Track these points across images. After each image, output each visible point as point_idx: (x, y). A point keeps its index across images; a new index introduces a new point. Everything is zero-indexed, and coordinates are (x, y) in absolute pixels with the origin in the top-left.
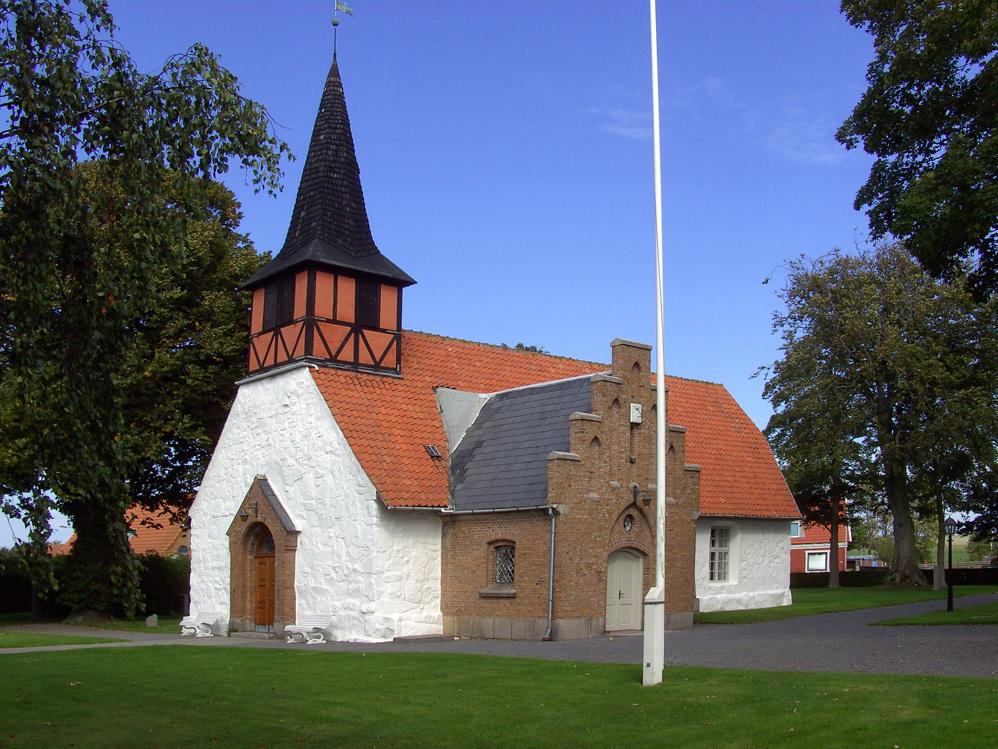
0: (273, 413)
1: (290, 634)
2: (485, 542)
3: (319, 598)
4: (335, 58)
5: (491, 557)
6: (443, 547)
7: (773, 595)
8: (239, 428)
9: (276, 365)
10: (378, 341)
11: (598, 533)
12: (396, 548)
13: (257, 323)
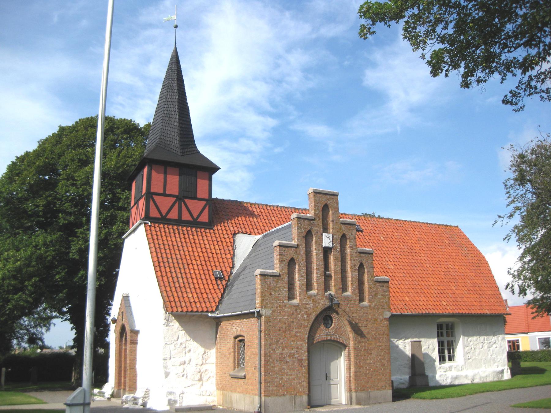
2: (232, 337)
4: (175, 45)
10: (196, 206)
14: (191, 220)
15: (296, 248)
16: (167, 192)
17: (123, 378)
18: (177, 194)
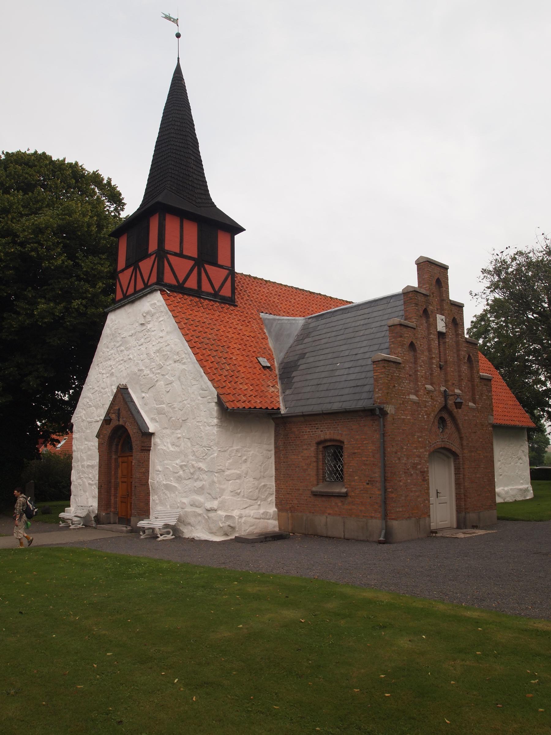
0: (133, 332)
1: (143, 530)
3: (169, 495)
5: (320, 456)
6: (276, 447)
7: (521, 490)
8: (108, 348)
9: (136, 292)
11: (419, 434)
12: (235, 448)
13: (122, 263)
14: (213, 292)
15: (131, 336)
16: (185, 253)
17: (112, 498)
18: (195, 255)
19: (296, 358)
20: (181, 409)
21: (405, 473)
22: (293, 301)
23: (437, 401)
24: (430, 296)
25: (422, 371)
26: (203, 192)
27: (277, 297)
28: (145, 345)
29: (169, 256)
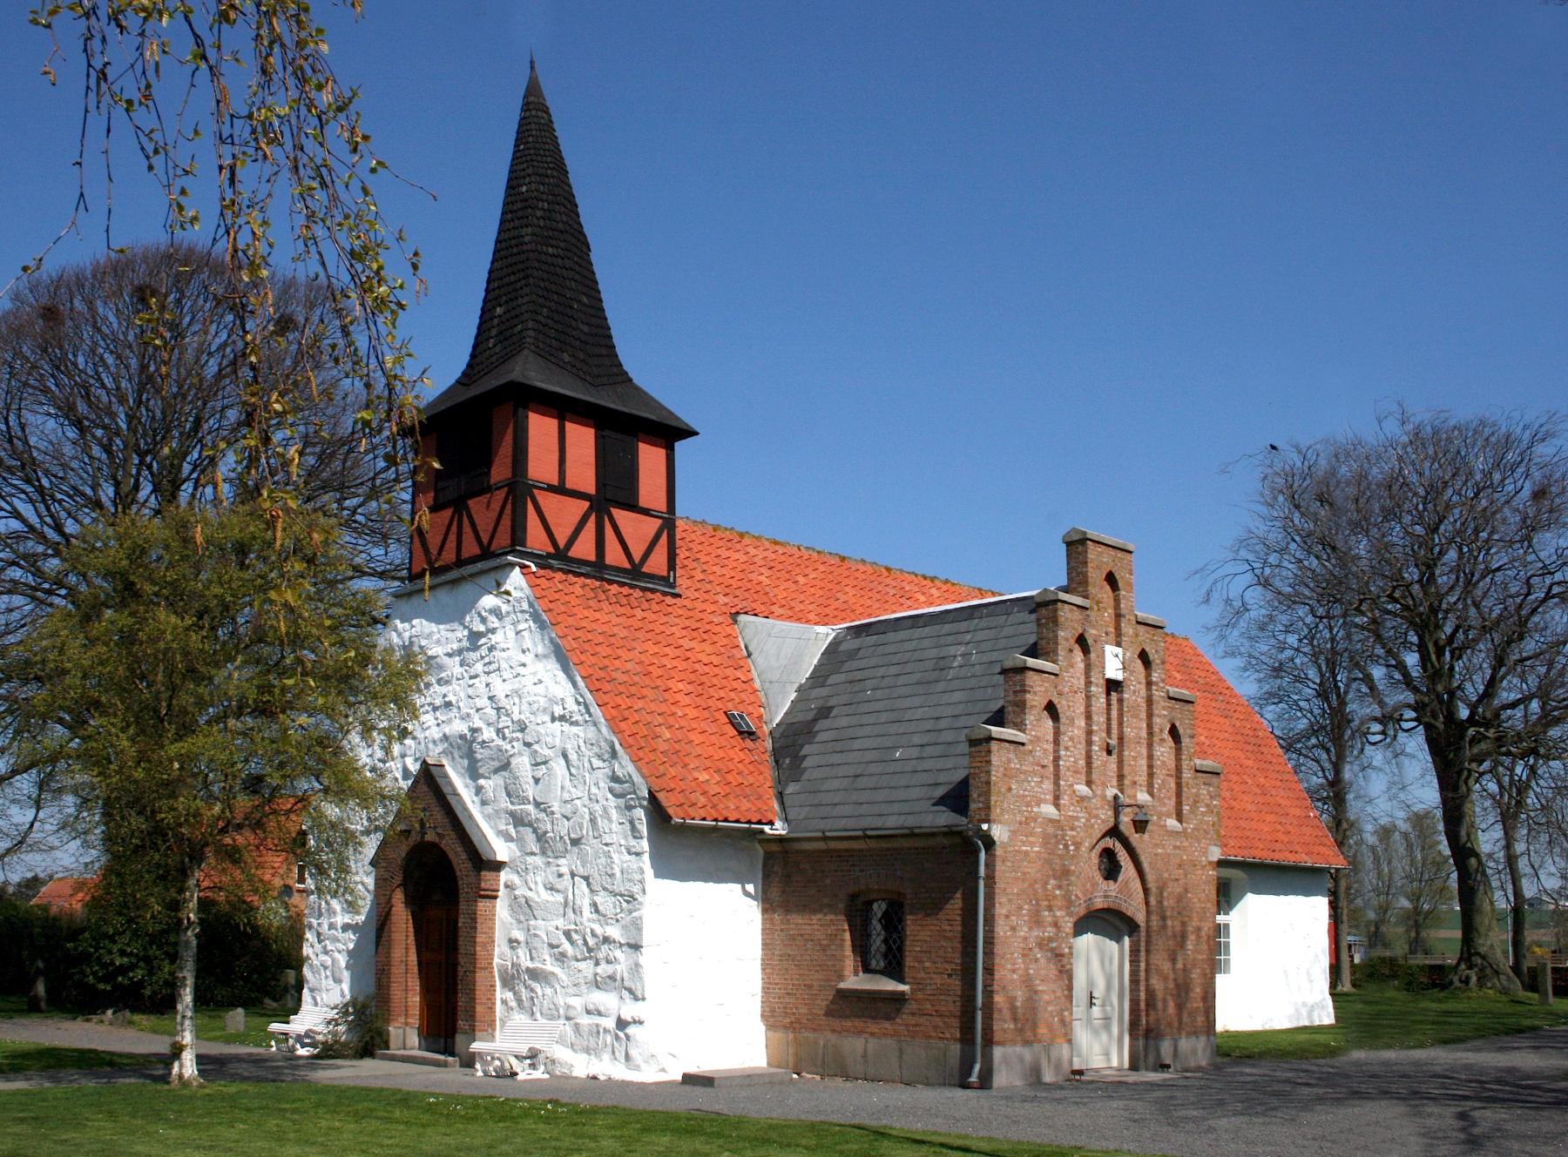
4: (532, 68)
9: (460, 563)
14: (627, 565)
16: (569, 485)
18: (591, 489)
19: (811, 716)
20: (570, 815)
21: (1023, 955)
22: (802, 580)
23: (1097, 817)
24: (1092, 609)
25: (1072, 757)
26: (604, 351)
27: (767, 572)
28: (484, 678)
29: (536, 491)
